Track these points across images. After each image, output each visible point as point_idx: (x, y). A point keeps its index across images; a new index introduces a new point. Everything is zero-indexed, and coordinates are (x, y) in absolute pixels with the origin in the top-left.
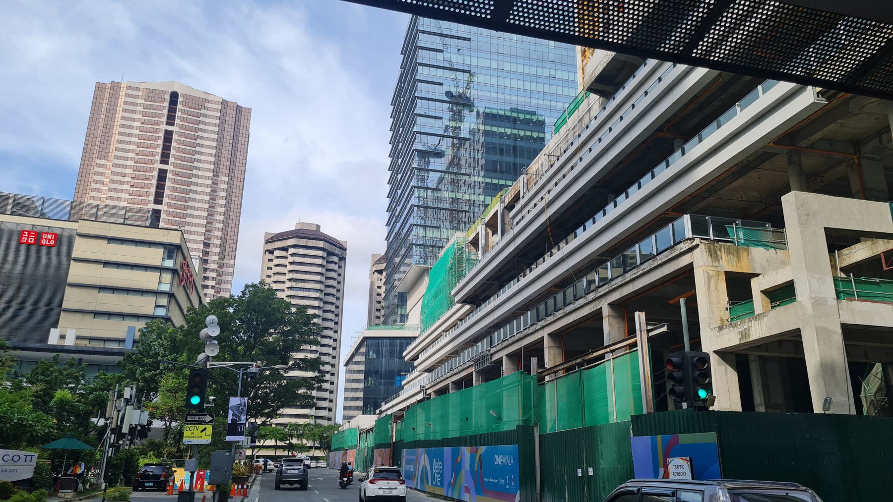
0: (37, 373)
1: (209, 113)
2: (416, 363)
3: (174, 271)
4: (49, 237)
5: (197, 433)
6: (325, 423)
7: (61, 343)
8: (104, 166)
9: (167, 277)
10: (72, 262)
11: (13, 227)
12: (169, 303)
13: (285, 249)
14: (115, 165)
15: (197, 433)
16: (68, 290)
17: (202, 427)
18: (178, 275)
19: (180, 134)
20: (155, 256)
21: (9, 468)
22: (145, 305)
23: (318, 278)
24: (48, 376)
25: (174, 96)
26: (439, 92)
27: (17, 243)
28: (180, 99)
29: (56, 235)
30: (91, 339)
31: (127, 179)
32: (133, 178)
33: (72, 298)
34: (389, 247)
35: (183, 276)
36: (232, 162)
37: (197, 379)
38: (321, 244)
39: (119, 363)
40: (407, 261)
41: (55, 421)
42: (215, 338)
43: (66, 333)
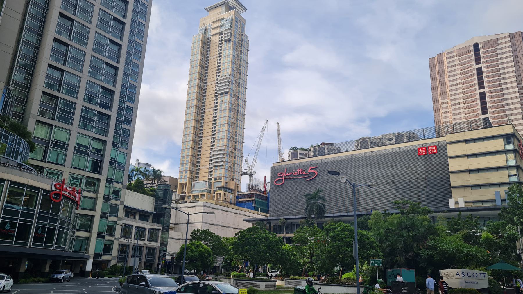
0: (452, 225)
1: (502, 46)
3: (514, 151)
4: (433, 148)
7: (457, 206)
8: (446, 103)
9: (511, 156)
10: (449, 159)
11: (413, 148)
12: (518, 172)
14: (452, 100)
16: (451, 176)
18: (519, 153)
19: (487, 67)
20: (499, 144)
21: (471, 281)
22: (502, 177)
24: (458, 226)
27: (417, 156)
28: (480, 46)
29: (436, 146)
30: (474, 202)
31: (461, 106)
32: (465, 104)
33: (455, 180)
39: (499, 214)
41: (488, 252)
43: (458, 200)
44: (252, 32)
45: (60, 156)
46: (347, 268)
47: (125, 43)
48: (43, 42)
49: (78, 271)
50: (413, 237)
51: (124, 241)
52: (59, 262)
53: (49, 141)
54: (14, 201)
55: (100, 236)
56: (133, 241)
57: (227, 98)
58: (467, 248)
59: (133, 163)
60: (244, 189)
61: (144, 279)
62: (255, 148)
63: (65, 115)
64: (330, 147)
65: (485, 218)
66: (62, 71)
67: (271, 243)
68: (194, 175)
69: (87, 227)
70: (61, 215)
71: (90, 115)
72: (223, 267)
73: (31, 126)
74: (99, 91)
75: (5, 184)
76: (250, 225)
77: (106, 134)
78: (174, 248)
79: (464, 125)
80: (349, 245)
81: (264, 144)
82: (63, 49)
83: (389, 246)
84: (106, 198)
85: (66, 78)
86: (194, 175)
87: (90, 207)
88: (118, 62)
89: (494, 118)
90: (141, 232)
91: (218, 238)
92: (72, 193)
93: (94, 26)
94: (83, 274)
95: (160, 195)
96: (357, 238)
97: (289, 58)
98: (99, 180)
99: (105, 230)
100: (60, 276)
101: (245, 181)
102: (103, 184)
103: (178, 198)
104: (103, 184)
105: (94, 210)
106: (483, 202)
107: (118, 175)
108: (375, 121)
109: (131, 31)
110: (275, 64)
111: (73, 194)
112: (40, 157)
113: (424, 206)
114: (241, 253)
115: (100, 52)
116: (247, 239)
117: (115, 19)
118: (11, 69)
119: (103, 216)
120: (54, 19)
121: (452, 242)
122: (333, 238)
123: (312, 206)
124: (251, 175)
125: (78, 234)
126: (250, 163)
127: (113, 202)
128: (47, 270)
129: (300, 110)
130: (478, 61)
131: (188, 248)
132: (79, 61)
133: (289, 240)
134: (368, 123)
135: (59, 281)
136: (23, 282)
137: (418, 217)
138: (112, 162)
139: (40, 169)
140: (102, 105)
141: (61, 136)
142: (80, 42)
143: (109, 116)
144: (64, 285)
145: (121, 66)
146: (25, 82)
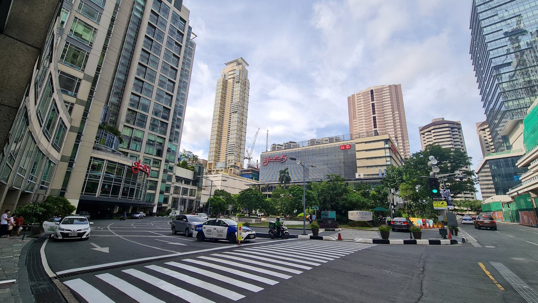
2: (529, 168)
3: (389, 148)
5: (440, 205)
6: (471, 200)
7: (359, 177)
9: (388, 151)
13: (430, 131)
15: (440, 205)
17: (442, 202)
19: (377, 103)
23: (449, 139)
25: (372, 91)
26: (501, 34)
30: (368, 175)
33: (359, 163)
34: (488, 118)
35: (393, 149)
36: (398, 106)
37: (433, 182)
38: (447, 125)
40: (504, 120)
42: (436, 165)
43: (360, 174)
44: (252, 78)
45: (138, 146)
46: (301, 210)
47: (177, 82)
48: (128, 80)
49: (148, 213)
50: (336, 194)
51: (175, 196)
52: (137, 208)
53: (131, 137)
54: (110, 172)
55: (161, 193)
56: (180, 196)
57: (236, 115)
58: (363, 199)
59: (181, 151)
60: (245, 167)
61: (185, 217)
62: (252, 143)
63: (140, 122)
64: (294, 144)
65: (374, 184)
66: (140, 97)
67: (259, 197)
68: (217, 159)
69: (154, 188)
70: (138, 181)
71: (156, 123)
72: (232, 211)
73: (121, 128)
74: (162, 109)
75: (105, 162)
76: (248, 187)
77: (165, 134)
78: (204, 200)
79: (365, 134)
80: (301, 199)
81: (257, 142)
82: (140, 84)
83: (323, 199)
84: (165, 171)
85: (142, 101)
86: (217, 159)
87: (156, 176)
88: (173, 92)
89: (380, 130)
90: (185, 191)
91: (229, 194)
92: (145, 168)
93: (159, 71)
94: (151, 214)
95: (197, 169)
96: (305, 194)
97: (272, 93)
98: (161, 160)
99: (164, 189)
100: (138, 215)
101: (246, 162)
102: (163, 162)
103: (207, 171)
104: (163, 162)
105: (158, 178)
106: (372, 175)
107: (172, 157)
108: (319, 130)
109: (181, 75)
110: (264, 96)
111: (145, 168)
112: (126, 147)
113: (343, 177)
114: (242, 203)
115: (162, 86)
116: (246, 195)
117: (172, 67)
118: (109, 95)
119: (163, 181)
120: (135, 66)
121: (356, 196)
122: (293, 194)
123: (283, 177)
124: (249, 159)
125: (148, 191)
126: (249, 152)
127: (169, 173)
128: (130, 212)
129: (279, 123)
130: (373, 99)
131: (212, 200)
132: (150, 92)
133: (270, 196)
134: (315, 131)
135: (137, 218)
136: (116, 219)
137: (339, 183)
138: (169, 150)
139: (126, 154)
140: (163, 117)
141: (139, 135)
142: (150, 80)
143: (167, 124)
144: (139, 221)
145: (175, 95)
146: (118, 103)
